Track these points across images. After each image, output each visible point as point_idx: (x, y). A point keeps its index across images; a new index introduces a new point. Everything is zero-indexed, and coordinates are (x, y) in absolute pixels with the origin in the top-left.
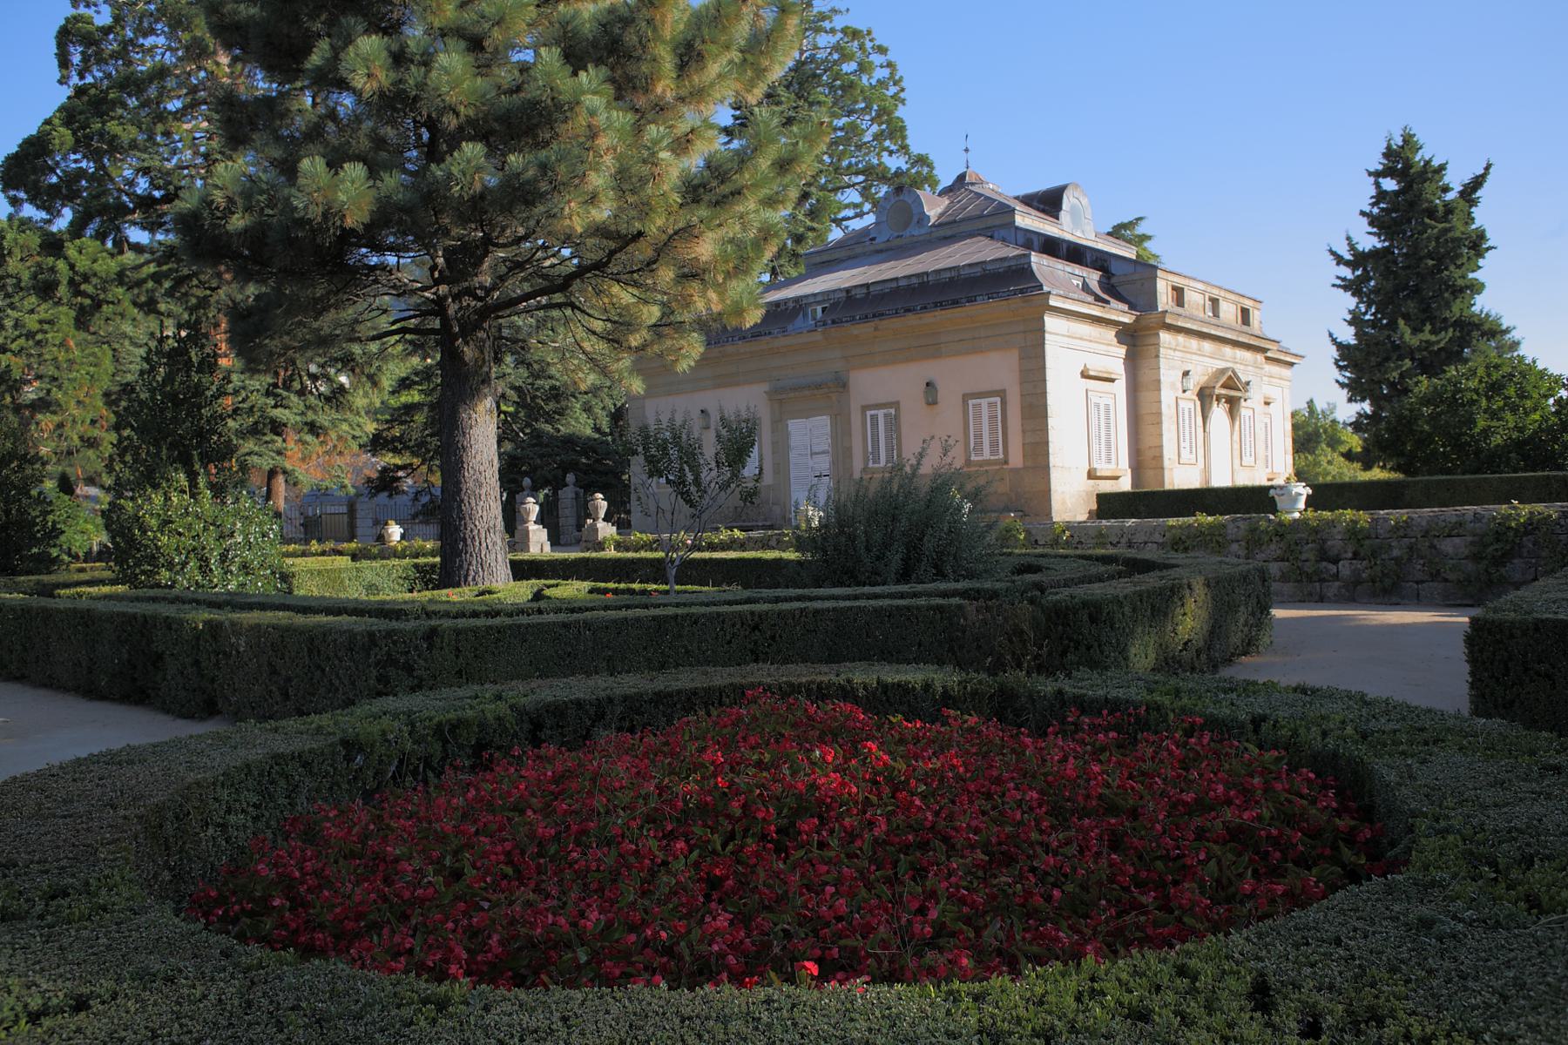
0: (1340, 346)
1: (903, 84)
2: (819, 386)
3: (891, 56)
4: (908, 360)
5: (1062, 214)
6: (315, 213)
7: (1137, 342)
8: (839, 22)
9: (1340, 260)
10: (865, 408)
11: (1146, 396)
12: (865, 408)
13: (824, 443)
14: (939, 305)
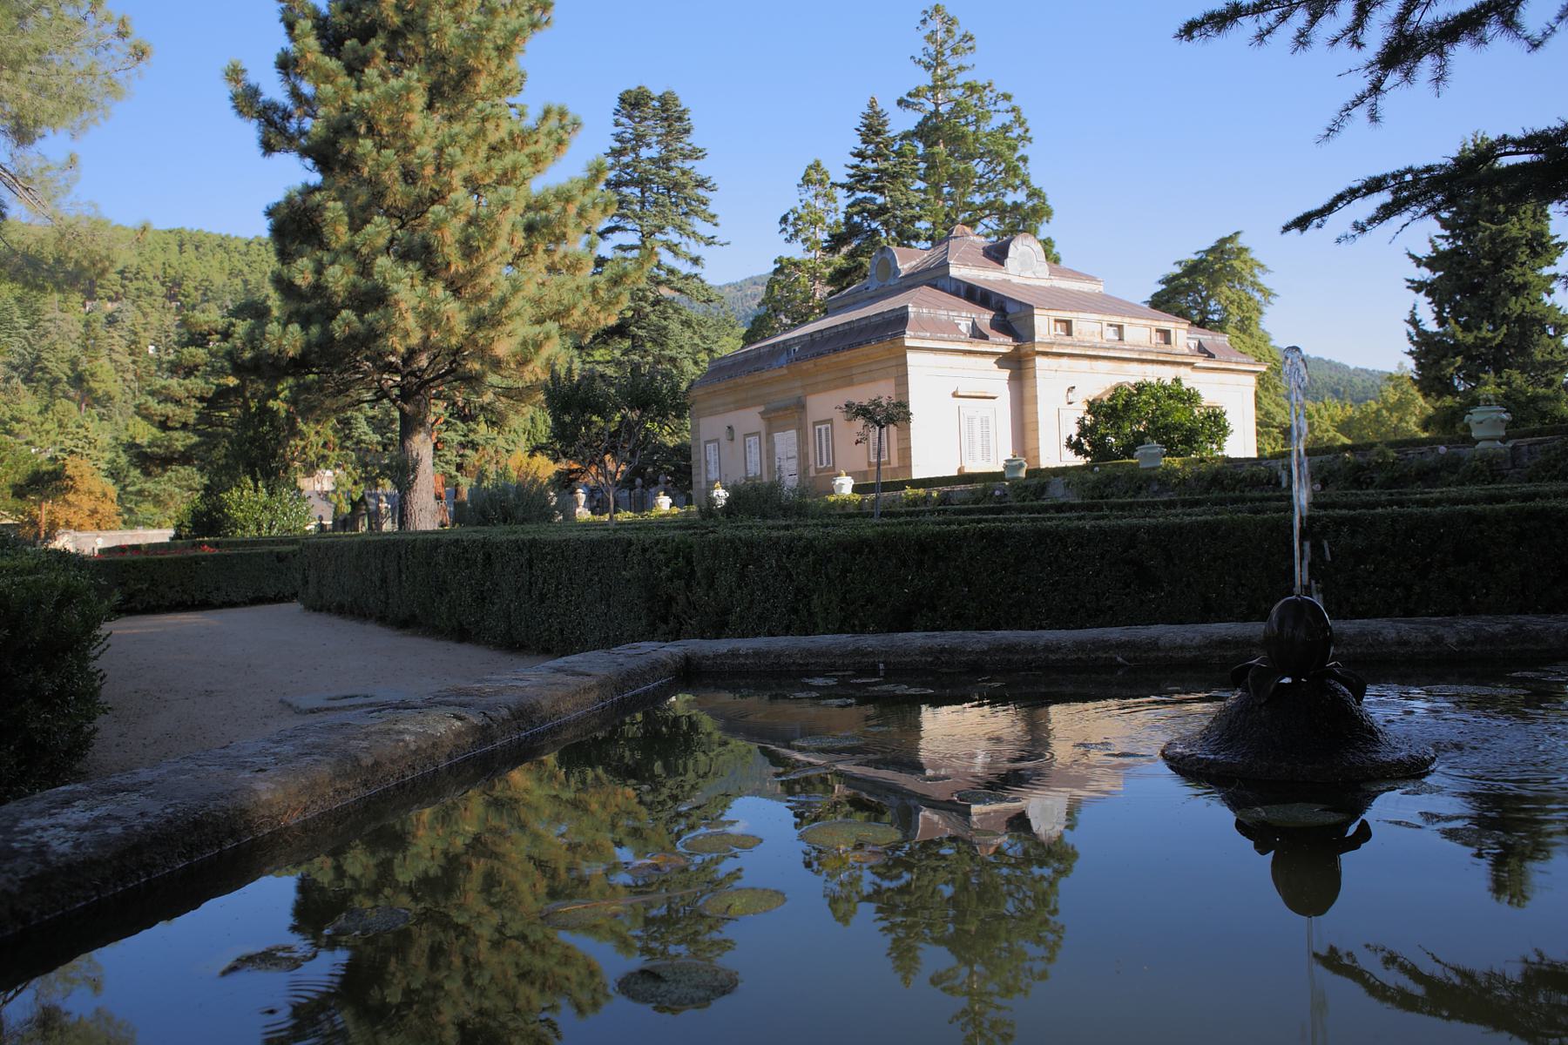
0: (1422, 333)
1: (1028, 125)
2: (786, 408)
3: (1015, 102)
4: (837, 387)
5: (1008, 261)
6: (274, 350)
7: (1018, 365)
8: (961, 79)
9: (1418, 262)
10: (815, 424)
11: (1028, 408)
12: (815, 424)
13: (794, 451)
14: (851, 347)
